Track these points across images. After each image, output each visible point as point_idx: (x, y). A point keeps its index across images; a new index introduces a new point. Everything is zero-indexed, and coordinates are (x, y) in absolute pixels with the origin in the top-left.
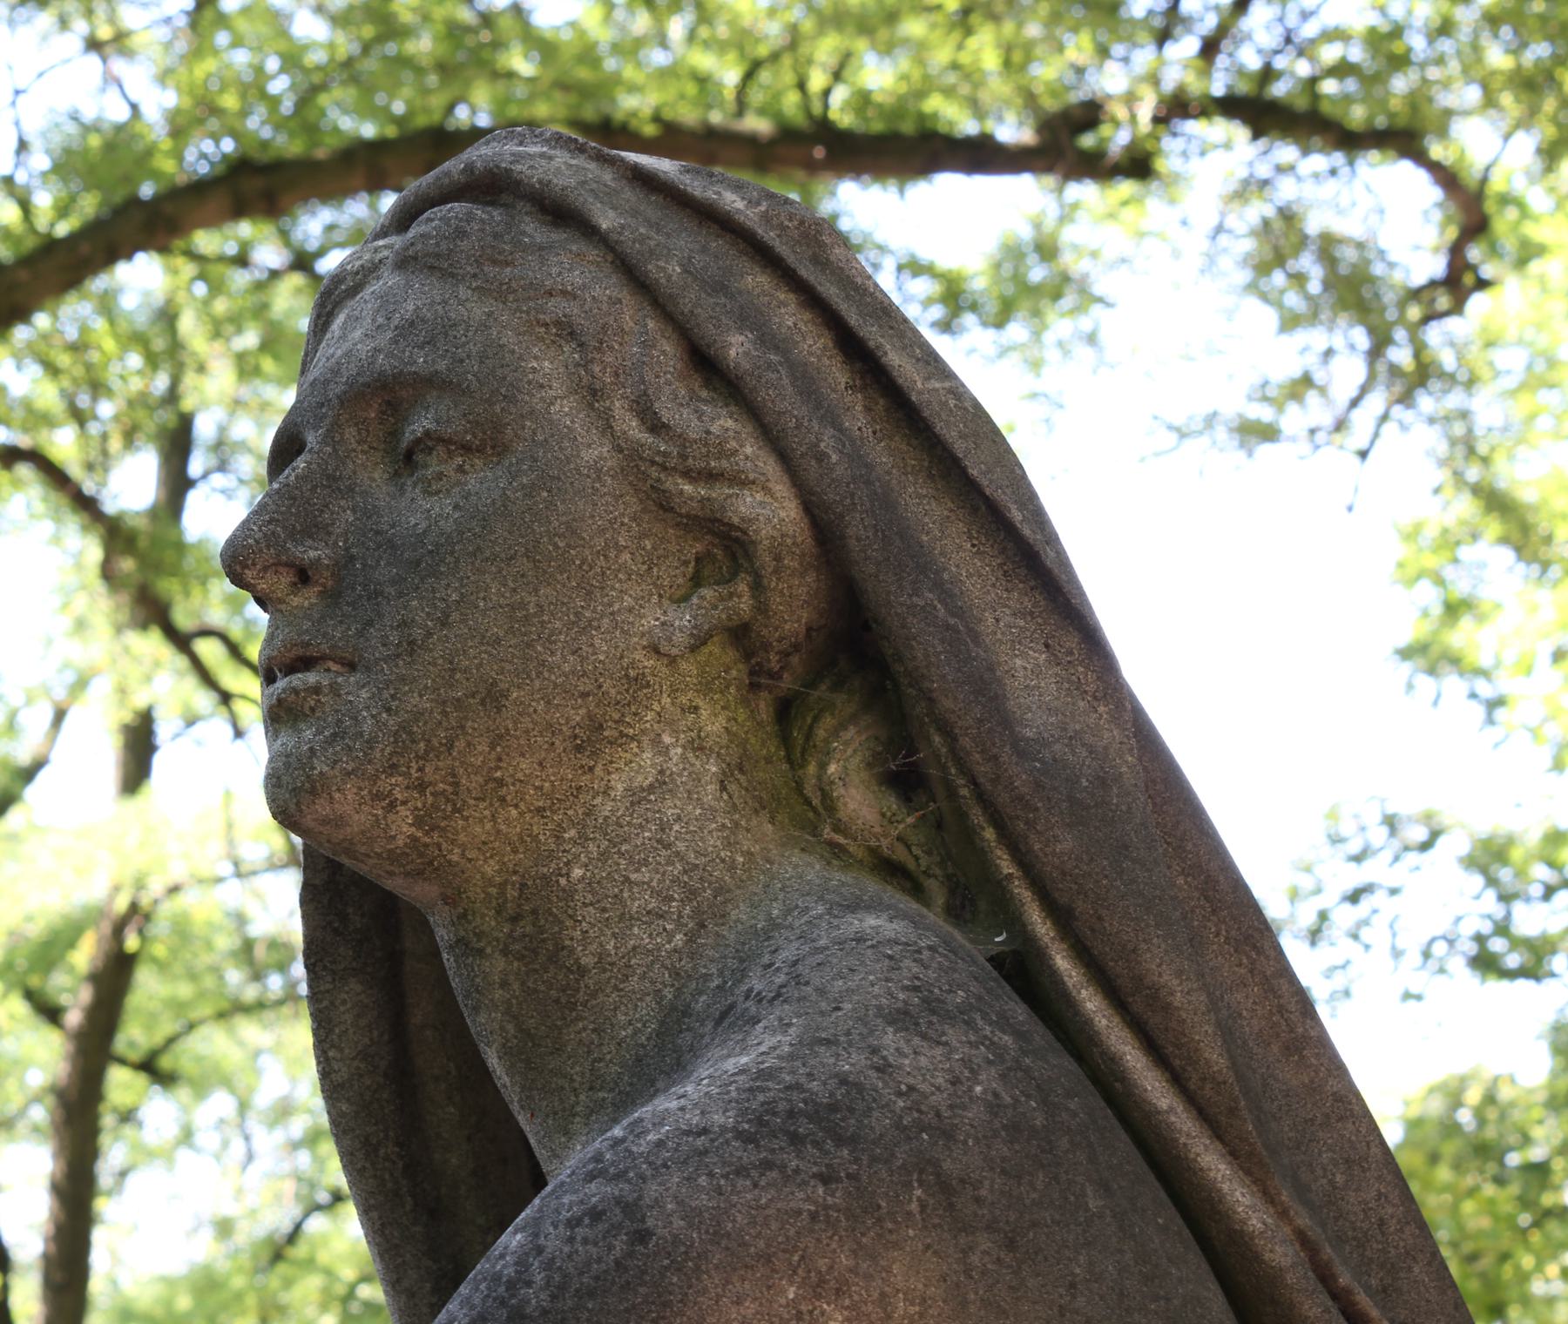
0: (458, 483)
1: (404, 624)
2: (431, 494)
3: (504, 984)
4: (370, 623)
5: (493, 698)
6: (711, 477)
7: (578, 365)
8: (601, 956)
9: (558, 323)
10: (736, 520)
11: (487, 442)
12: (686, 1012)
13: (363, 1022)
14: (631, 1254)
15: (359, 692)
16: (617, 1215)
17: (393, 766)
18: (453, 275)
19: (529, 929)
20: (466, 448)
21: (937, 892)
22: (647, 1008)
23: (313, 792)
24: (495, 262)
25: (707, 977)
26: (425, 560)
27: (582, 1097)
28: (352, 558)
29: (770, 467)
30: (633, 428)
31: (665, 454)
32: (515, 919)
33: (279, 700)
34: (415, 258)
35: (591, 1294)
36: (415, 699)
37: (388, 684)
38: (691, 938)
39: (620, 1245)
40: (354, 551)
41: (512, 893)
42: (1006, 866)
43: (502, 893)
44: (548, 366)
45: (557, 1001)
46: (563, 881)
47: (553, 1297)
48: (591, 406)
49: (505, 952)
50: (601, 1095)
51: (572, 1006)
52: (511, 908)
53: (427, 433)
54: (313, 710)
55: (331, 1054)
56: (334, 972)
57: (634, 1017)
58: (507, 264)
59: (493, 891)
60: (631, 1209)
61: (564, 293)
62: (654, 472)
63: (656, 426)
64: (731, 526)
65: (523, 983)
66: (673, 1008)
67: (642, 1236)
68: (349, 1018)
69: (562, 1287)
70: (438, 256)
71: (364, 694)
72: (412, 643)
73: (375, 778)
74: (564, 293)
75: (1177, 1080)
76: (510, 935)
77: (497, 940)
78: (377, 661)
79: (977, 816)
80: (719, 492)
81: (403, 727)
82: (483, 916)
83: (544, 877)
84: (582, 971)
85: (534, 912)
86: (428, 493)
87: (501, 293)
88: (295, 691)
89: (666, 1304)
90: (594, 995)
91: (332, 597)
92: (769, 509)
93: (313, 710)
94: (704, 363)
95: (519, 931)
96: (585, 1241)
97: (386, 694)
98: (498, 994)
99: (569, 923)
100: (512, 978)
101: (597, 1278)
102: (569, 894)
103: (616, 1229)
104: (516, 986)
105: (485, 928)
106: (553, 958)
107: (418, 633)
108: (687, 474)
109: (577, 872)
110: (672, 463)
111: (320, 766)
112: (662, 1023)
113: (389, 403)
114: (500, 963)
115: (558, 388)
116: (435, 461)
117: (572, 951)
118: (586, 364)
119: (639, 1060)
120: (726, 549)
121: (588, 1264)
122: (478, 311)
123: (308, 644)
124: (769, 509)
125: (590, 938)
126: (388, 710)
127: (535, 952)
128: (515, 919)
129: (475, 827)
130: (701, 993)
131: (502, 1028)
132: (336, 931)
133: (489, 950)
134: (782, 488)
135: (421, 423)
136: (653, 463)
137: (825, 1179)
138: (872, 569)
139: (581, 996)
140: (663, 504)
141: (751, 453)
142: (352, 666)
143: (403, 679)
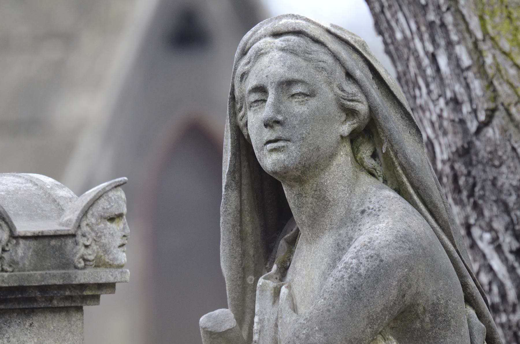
6: (352, 101)
15: (292, 147)
16: (375, 257)
18: (297, 55)
20: (307, 95)
21: (381, 179)
24: (307, 53)
25: (354, 203)
27: (328, 226)
28: (287, 118)
32: (316, 191)
38: (350, 194)
39: (378, 262)
42: (405, 179)
51: (327, 208)
60: (378, 255)
63: (343, 90)
66: (348, 209)
67: (382, 261)
69: (368, 270)
70: (293, 50)
71: (293, 147)
74: (323, 61)
75: (436, 221)
79: (399, 168)
85: (320, 190)
92: (362, 108)
94: (349, 75)
96: (371, 261)
98: (309, 205)
102: (327, 186)
103: (376, 259)
106: (324, 199)
109: (328, 182)
110: (346, 98)
114: (311, 199)
119: (341, 219)
124: (362, 108)
134: (365, 103)
137: (410, 249)
139: (329, 206)
141: (360, 96)
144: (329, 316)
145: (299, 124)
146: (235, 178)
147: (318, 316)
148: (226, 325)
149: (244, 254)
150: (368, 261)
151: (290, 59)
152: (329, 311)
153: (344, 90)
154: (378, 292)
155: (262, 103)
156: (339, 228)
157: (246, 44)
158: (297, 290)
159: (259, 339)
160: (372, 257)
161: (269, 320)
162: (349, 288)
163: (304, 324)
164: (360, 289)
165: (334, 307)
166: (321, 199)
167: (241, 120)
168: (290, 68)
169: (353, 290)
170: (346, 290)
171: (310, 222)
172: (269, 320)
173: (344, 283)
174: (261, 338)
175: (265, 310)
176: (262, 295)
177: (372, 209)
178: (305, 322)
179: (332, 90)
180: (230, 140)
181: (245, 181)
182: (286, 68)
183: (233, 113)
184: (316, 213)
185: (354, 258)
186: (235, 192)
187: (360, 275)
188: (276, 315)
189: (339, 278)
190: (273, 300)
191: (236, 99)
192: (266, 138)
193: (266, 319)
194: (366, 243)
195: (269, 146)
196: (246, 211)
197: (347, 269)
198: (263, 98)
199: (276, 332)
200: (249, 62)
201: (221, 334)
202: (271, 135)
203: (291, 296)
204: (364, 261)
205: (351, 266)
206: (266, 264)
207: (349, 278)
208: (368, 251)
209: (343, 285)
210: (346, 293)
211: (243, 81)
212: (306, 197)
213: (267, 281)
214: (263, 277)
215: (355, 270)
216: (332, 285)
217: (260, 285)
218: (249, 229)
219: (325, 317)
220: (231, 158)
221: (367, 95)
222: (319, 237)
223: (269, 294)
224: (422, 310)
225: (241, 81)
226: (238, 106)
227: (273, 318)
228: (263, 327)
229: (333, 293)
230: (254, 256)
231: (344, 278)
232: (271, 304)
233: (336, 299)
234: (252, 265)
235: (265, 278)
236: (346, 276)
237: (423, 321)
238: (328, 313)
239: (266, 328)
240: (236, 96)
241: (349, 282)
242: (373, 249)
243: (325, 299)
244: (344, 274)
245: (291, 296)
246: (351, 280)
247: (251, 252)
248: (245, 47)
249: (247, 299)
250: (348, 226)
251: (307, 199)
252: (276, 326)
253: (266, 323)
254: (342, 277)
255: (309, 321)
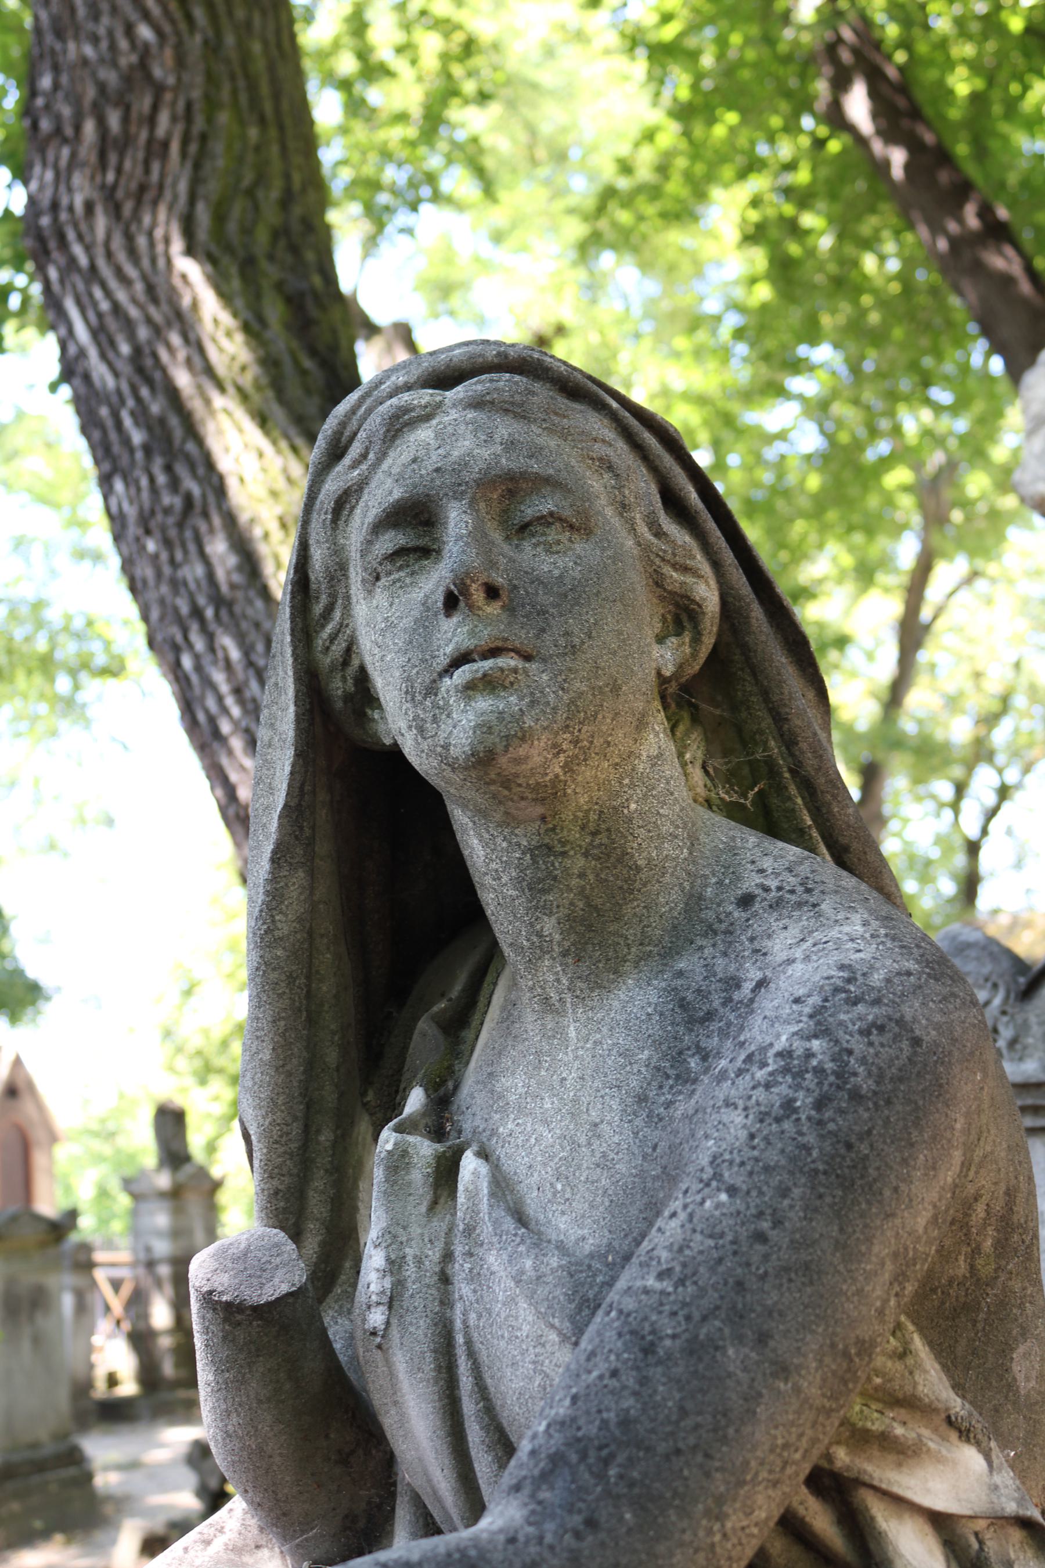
0: (570, 549)
1: (567, 634)
2: (552, 553)
3: (582, 875)
4: (543, 630)
5: (616, 689)
6: (685, 569)
7: (613, 487)
8: (649, 860)
9: (601, 459)
10: (698, 598)
11: (580, 526)
12: (701, 898)
13: (302, 897)
14: (915, 1053)
15: (540, 675)
17: (567, 726)
18: (524, 417)
19: (605, 841)
22: (675, 895)
23: (523, 739)
24: (556, 414)
26: (571, 595)
27: (633, 950)
29: (706, 569)
30: (643, 529)
31: (665, 551)
32: (594, 834)
33: (485, 675)
34: (492, 403)
35: (901, 1080)
36: (578, 685)
37: (561, 672)
40: (515, 582)
41: (593, 817)
43: (586, 817)
44: (597, 484)
45: (621, 888)
46: (626, 811)
47: (878, 1083)
48: (621, 514)
49: (586, 855)
50: (648, 948)
51: (631, 891)
52: (592, 826)
53: (551, 514)
54: (512, 684)
55: (277, 918)
56: (291, 864)
57: (669, 900)
58: (564, 417)
59: (580, 814)
60: (900, 1022)
61: (604, 441)
62: (657, 561)
63: (659, 533)
64: (693, 601)
65: (597, 875)
66: (692, 896)
67: (916, 1042)
68: (295, 894)
70: (512, 403)
72: (573, 647)
73: (557, 734)
76: (590, 844)
77: (580, 846)
78: (551, 656)
79: (793, 790)
80: (690, 580)
81: (572, 702)
82: (570, 830)
83: (614, 808)
84: (638, 869)
85: (608, 830)
86: (549, 551)
87: (564, 434)
88: (502, 670)
89: (941, 1086)
90: (645, 885)
91: (510, 609)
92: (707, 594)
93: (512, 684)
95: (597, 842)
96: (882, 1045)
97: (560, 679)
98: (575, 882)
99: (630, 838)
100: (589, 871)
101: (900, 1070)
104: (591, 877)
105: (571, 838)
106: (619, 860)
107: (577, 641)
108: (674, 566)
109: (633, 806)
110: (668, 557)
111: (529, 722)
112: (687, 904)
113: (510, 491)
114: (581, 862)
115: (603, 501)
116: (553, 533)
117: (632, 856)
118: (620, 488)
119: (675, 927)
120: (682, 614)
121: (892, 1060)
122: (553, 443)
123: (506, 639)
124: (707, 594)
125: (643, 850)
126: (563, 689)
127: (609, 857)
128: (594, 834)
129: (586, 773)
130: (706, 886)
131: (572, 904)
132: (296, 837)
133: (572, 853)
134: (713, 583)
135: (546, 504)
136: (658, 555)
138: (763, 638)
139: (637, 885)
140: (658, 582)
142: (528, 658)
143: (570, 670)
144: (766, 1257)
145: (558, 605)
146: (301, 828)
147: (720, 1261)
148: (276, 1280)
149: (312, 1065)
150: (871, 1044)
151: (505, 428)
152: (760, 1237)
153: (665, 534)
154: (921, 1157)
155: (420, 558)
156: (670, 953)
157: (343, 424)
158: (516, 1160)
159: (388, 1323)
160: (881, 1029)
161: (419, 1261)
162: (827, 1146)
163: (662, 1292)
164: (864, 1149)
165: (777, 1223)
166: (612, 860)
167: (328, 648)
168: (510, 445)
169: (843, 1151)
170: (815, 1153)
171: (573, 937)
172: (419, 1261)
173: (805, 1129)
174: (394, 1321)
175: (404, 1228)
176: (395, 1182)
177: (779, 889)
178: (667, 1285)
179: (633, 530)
180: (292, 709)
181: (323, 848)
182: (499, 449)
183: (302, 630)
184: (596, 908)
185: (816, 1036)
186: (301, 874)
187: (856, 1096)
188: (440, 1245)
189: (777, 1110)
190: (429, 1197)
191: (313, 586)
192: (449, 650)
193: (409, 1258)
194: (840, 983)
195: (463, 674)
196: (322, 936)
197: (800, 1074)
198: (420, 542)
199: (446, 1302)
200: (364, 456)
201: (259, 1311)
202: (472, 633)
203: (502, 1185)
204: (858, 1045)
205: (814, 1062)
206: (364, 1094)
207: (820, 1104)
208: (861, 1008)
209: (801, 1134)
210: (821, 1167)
211: (341, 523)
212: (564, 854)
213: (411, 1139)
214: (391, 1124)
215: (832, 1078)
216: (752, 1136)
217: (389, 1152)
218: (326, 988)
219: (748, 1264)
220: (293, 766)
221: (716, 565)
222: (600, 987)
223: (419, 1176)
224: (982, 1215)
225: (335, 520)
226: (318, 609)
227: (434, 1254)
228: (399, 1285)
229: (767, 1169)
230: (338, 1069)
231: (796, 1110)
232: (423, 1209)
233: (784, 1192)
234: (329, 1096)
235: (398, 1129)
236: (802, 1100)
237: (977, 1251)
238: (760, 1248)
239: (412, 1287)
240: (312, 578)
241: (820, 1123)
242: (877, 1002)
243: (732, 1191)
244: (791, 1093)
245: (502, 1185)
246: (828, 1114)
247: (332, 1056)
248: (342, 434)
249: (311, 1193)
250: (701, 948)
251: (568, 862)
252: (445, 1279)
253: (410, 1270)
254: (788, 1105)
255: (681, 1282)
